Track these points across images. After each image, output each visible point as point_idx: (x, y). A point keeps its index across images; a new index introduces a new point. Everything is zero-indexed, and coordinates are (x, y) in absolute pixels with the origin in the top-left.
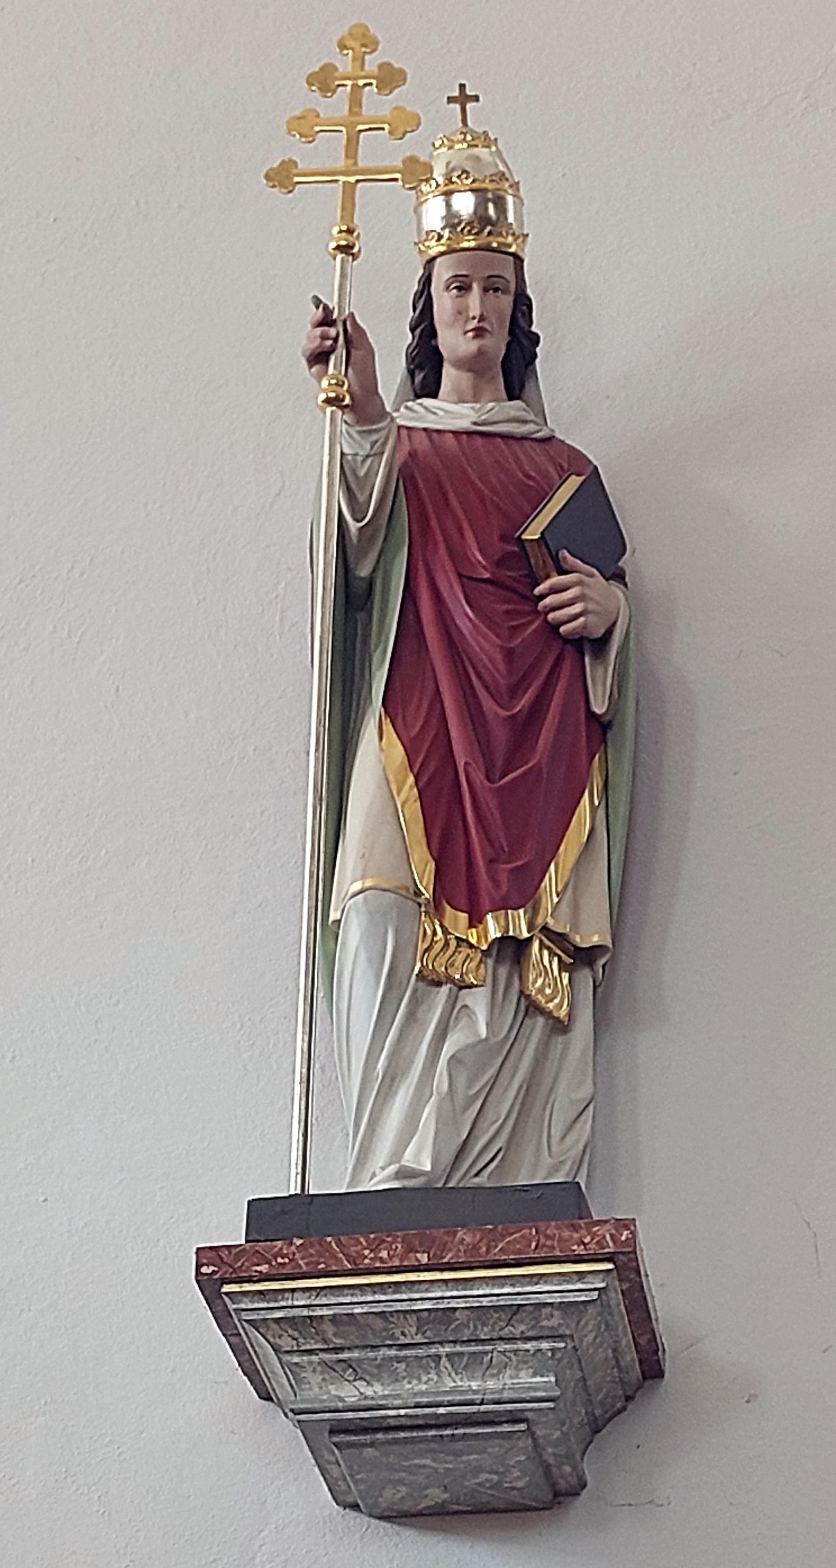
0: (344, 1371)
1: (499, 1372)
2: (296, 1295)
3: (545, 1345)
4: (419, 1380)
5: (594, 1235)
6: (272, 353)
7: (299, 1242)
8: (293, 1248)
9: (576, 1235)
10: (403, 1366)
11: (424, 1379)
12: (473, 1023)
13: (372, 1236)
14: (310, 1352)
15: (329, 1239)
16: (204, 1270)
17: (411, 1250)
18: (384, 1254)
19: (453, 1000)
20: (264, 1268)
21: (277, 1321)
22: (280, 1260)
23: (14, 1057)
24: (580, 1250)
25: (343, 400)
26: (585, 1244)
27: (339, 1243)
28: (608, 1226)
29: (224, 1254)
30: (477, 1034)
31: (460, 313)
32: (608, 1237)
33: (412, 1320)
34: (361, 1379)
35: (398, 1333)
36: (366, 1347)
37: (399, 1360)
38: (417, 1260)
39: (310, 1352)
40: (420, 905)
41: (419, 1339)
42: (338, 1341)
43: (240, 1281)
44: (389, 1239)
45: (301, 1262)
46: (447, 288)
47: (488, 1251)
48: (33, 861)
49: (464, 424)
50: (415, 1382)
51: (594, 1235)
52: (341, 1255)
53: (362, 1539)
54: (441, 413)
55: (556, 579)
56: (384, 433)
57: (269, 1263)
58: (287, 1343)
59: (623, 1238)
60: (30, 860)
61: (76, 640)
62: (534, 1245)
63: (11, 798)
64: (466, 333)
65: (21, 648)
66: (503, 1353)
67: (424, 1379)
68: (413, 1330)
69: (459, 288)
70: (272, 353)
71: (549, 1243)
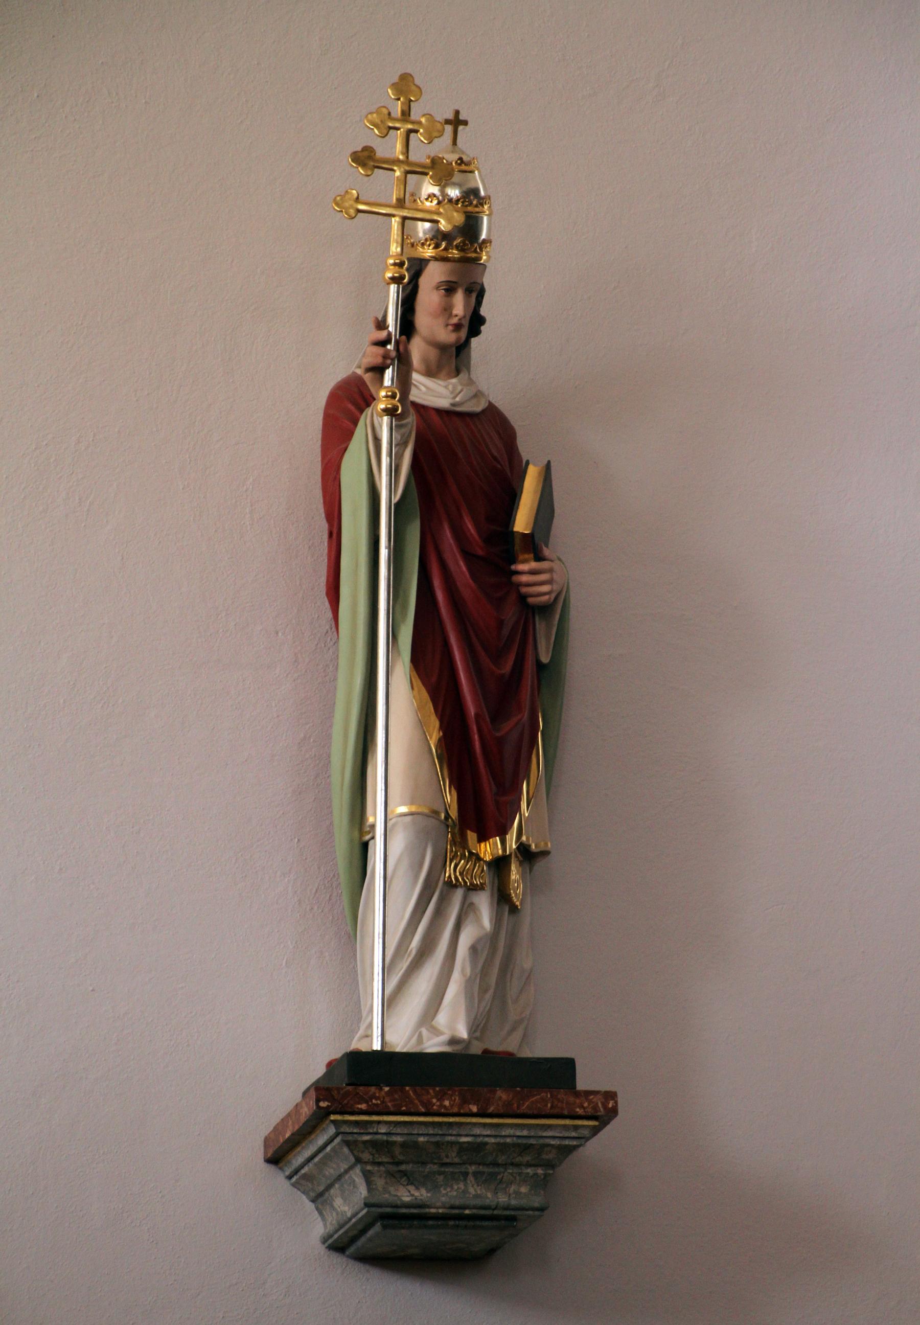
0: (401, 1178)
1: (507, 1187)
2: (380, 1126)
3: (540, 1171)
4: (452, 1188)
5: (590, 1102)
6: (232, 262)
7: (387, 1089)
8: (383, 1093)
9: (578, 1101)
10: (442, 1177)
11: (456, 1187)
12: (478, 920)
13: (437, 1089)
14: (379, 1164)
15: (407, 1088)
16: (322, 1104)
17: (465, 1101)
18: (447, 1103)
19: (465, 898)
20: (363, 1106)
21: (365, 1142)
22: (374, 1101)
23: (61, 869)
24: (579, 1111)
25: (397, 410)
26: (584, 1108)
27: (415, 1092)
28: (599, 1096)
29: (335, 1093)
30: (482, 927)
31: (445, 310)
32: (600, 1105)
33: (455, 1149)
34: (412, 1184)
35: (443, 1155)
36: (418, 1163)
37: (440, 1173)
38: (470, 1110)
39: (379, 1164)
40: (448, 826)
41: (457, 1160)
42: (401, 1158)
43: (341, 1113)
44: (450, 1092)
45: (389, 1104)
46: (437, 288)
47: (518, 1107)
48: (64, 702)
49: (443, 403)
50: (449, 1190)
51: (590, 1102)
52: (416, 1101)
53: (342, 1273)
54: (423, 388)
55: (533, 565)
56: (410, 426)
57: (367, 1102)
58: (366, 1156)
59: (610, 1105)
60: (62, 701)
61: (85, 509)
62: (549, 1105)
63: (42, 644)
64: (447, 325)
65: (41, 509)
66: (511, 1174)
67: (456, 1187)
68: (454, 1154)
69: (446, 290)
70: (232, 262)
71: (559, 1105)
